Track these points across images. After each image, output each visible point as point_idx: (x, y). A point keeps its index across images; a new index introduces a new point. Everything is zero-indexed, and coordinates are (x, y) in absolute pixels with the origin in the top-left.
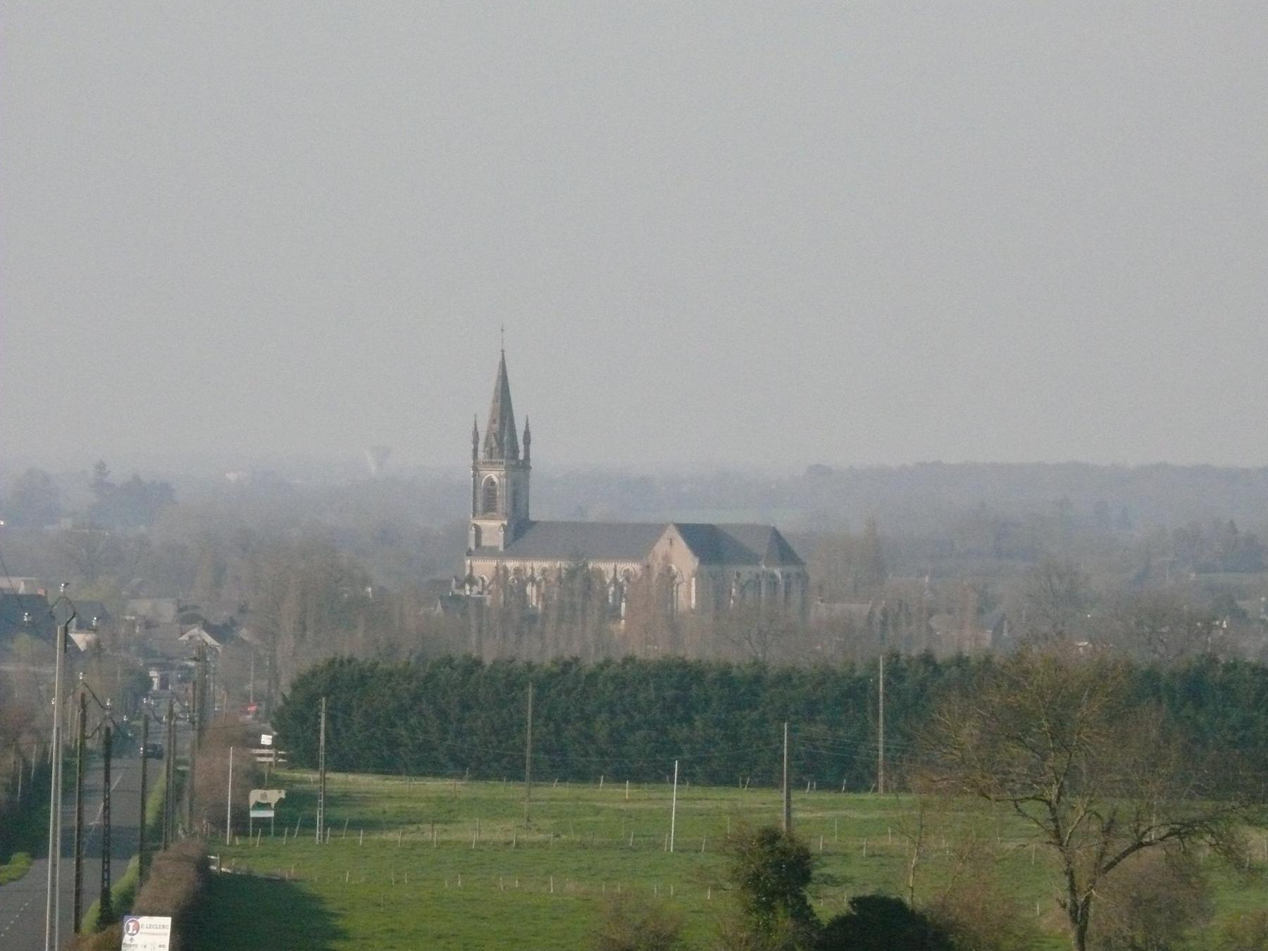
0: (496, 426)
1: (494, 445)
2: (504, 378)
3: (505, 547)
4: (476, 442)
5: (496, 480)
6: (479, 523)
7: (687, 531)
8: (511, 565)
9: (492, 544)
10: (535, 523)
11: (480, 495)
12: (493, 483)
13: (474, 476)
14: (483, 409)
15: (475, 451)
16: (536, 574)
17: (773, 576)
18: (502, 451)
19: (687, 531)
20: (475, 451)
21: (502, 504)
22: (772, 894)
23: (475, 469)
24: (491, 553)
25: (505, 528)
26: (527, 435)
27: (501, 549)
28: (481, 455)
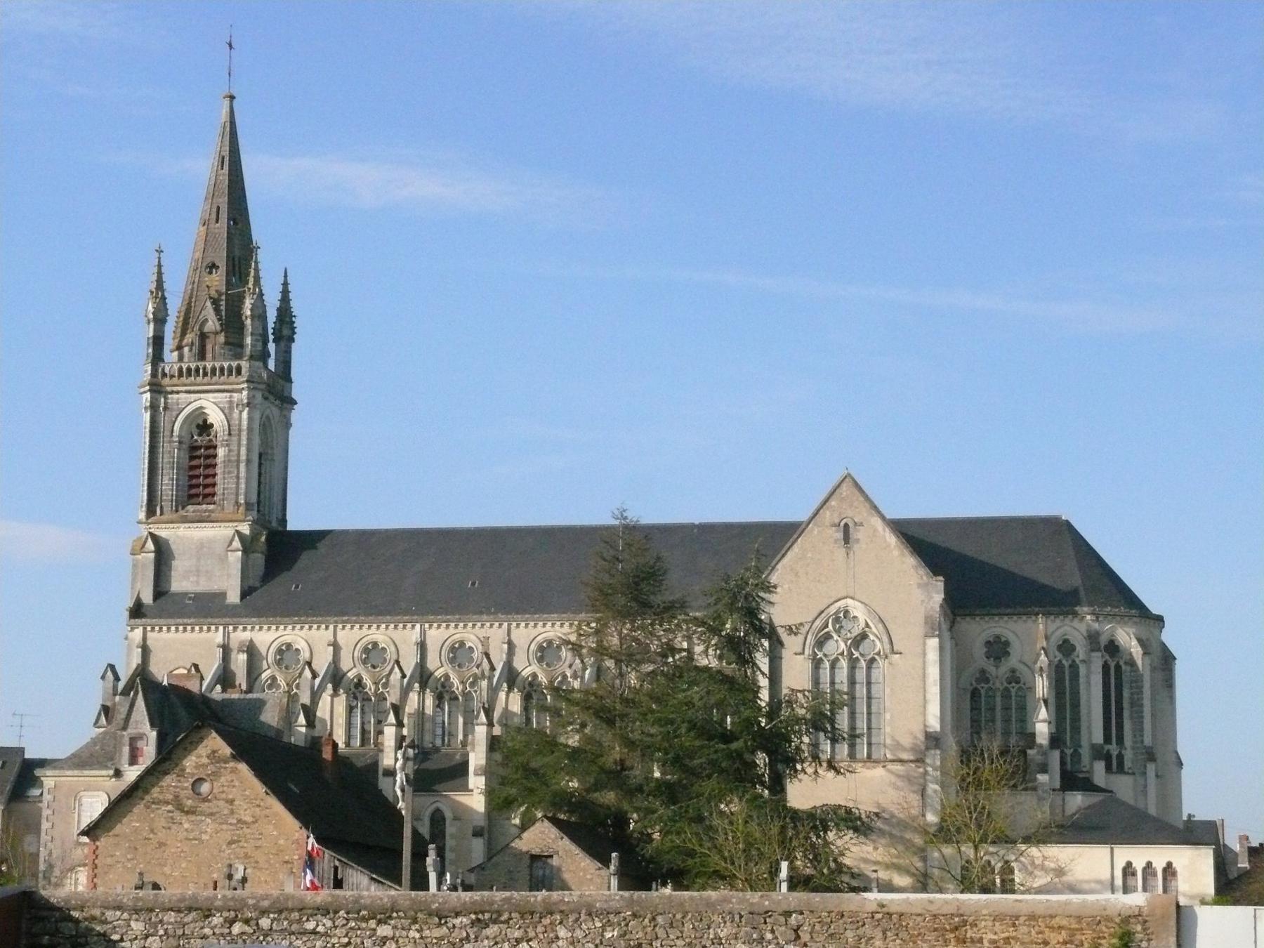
0: (217, 280)
1: (212, 324)
2: (285, 284)
3: (244, 595)
4: (160, 320)
5: (216, 417)
6: (164, 532)
7: (928, 544)
8: (267, 637)
9: (203, 586)
10: (311, 539)
11: (171, 453)
12: (205, 427)
13: (154, 407)
14: (181, 242)
15: (158, 341)
16: (345, 664)
17: (1113, 648)
18: (234, 346)
19: (928, 544)
20: (158, 341)
21: (233, 480)
22: (623, 769)
23: (156, 388)
24: (206, 607)
25: (248, 545)
26: (285, 314)
27: (234, 597)
28: (170, 356)
